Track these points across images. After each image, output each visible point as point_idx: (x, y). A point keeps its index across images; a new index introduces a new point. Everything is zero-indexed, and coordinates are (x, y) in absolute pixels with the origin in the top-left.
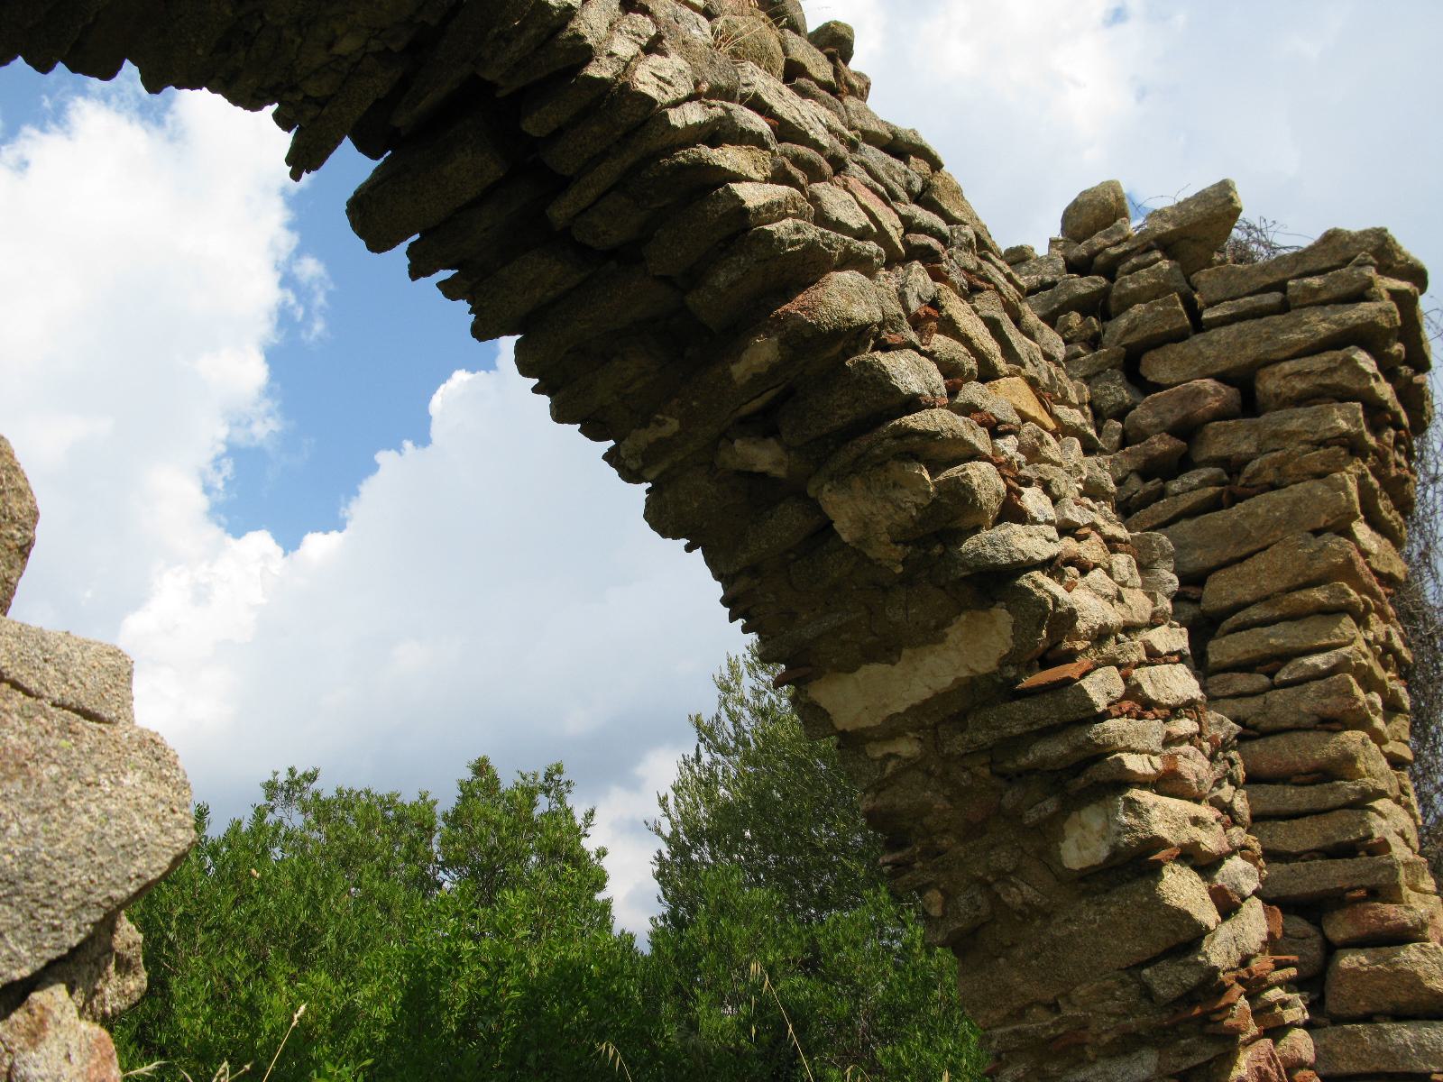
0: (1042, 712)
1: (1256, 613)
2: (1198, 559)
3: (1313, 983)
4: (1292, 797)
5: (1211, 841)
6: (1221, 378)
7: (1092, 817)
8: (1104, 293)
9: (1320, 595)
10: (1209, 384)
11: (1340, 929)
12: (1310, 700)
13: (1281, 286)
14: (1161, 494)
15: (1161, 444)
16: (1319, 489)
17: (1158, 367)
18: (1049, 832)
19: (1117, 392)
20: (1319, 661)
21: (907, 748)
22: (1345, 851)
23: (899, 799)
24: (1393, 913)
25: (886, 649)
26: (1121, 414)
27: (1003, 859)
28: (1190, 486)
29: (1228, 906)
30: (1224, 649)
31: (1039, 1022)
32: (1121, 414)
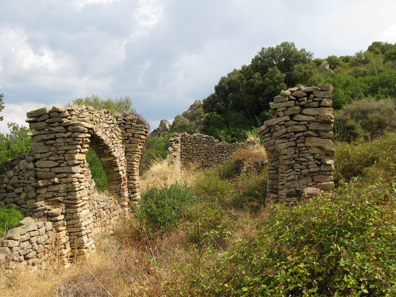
0: (114, 162)
1: (130, 152)
2: (127, 147)
3: (128, 177)
4: (130, 166)
5: (123, 169)
6: (132, 133)
7: (116, 168)
8: (125, 123)
9: (134, 152)
10: (130, 134)
11: (131, 174)
12: (132, 159)
13: (138, 128)
14: (125, 141)
15: (126, 138)
16: (136, 145)
17: (128, 131)
18: (113, 169)
19: (124, 132)
20: (133, 157)
21: (106, 162)
22: (132, 170)
23: (105, 165)
24: (134, 174)
25: (106, 157)
26: (124, 134)
27: (110, 169)
28: (128, 141)
29: (123, 173)
30: (127, 154)
31: (111, 179)
32: (124, 134)
